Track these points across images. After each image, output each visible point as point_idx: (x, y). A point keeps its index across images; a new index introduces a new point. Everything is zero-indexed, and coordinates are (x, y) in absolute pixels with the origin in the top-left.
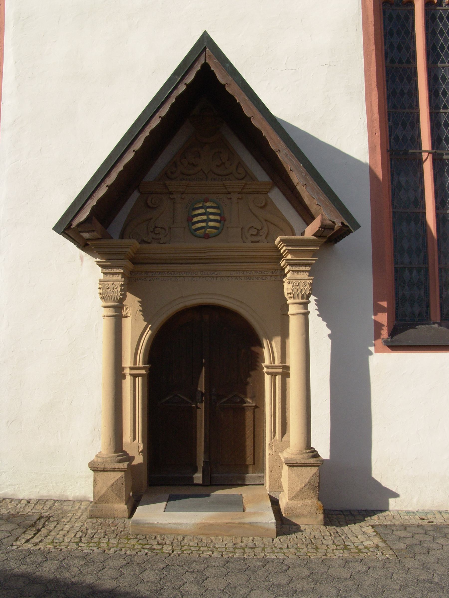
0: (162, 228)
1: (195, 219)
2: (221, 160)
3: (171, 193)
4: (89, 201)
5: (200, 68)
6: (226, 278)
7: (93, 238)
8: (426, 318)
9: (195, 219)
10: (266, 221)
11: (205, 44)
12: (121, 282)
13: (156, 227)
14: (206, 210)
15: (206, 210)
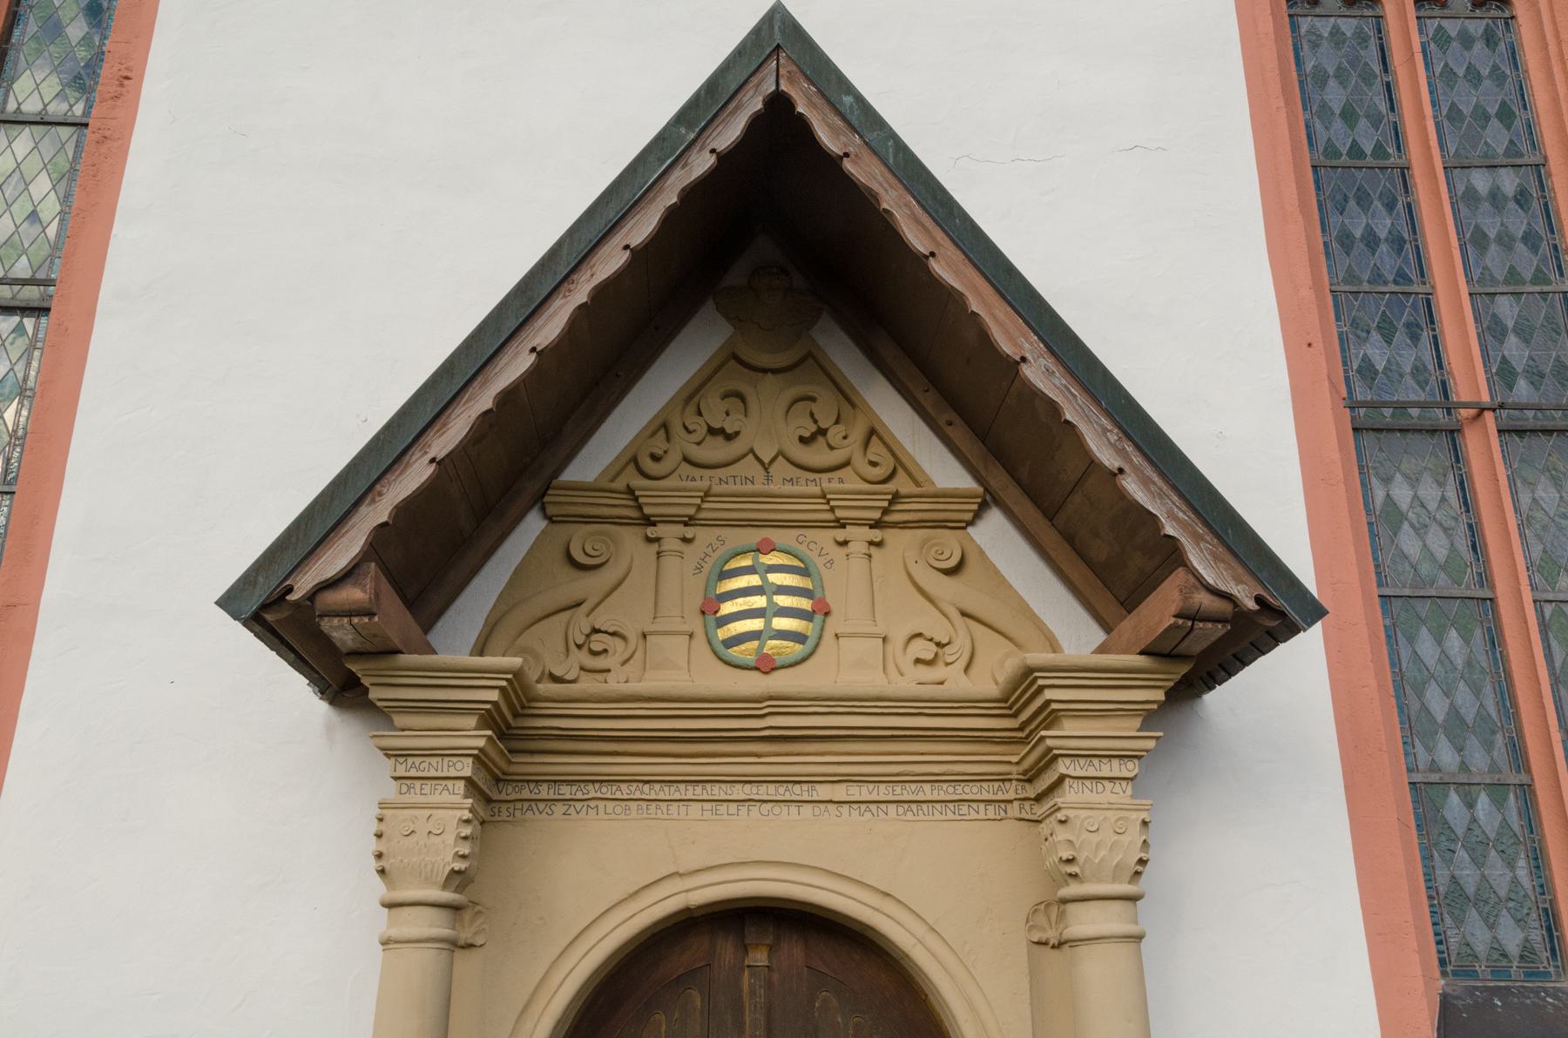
0: (614, 634)
1: (728, 608)
2: (815, 422)
3: (649, 521)
4: (363, 509)
5: (760, 106)
6: (830, 806)
7: (369, 647)
8: (1551, 969)
9: (728, 608)
10: (964, 614)
11: (779, 39)
12: (458, 813)
13: (596, 631)
14: (764, 579)
15: (764, 579)
